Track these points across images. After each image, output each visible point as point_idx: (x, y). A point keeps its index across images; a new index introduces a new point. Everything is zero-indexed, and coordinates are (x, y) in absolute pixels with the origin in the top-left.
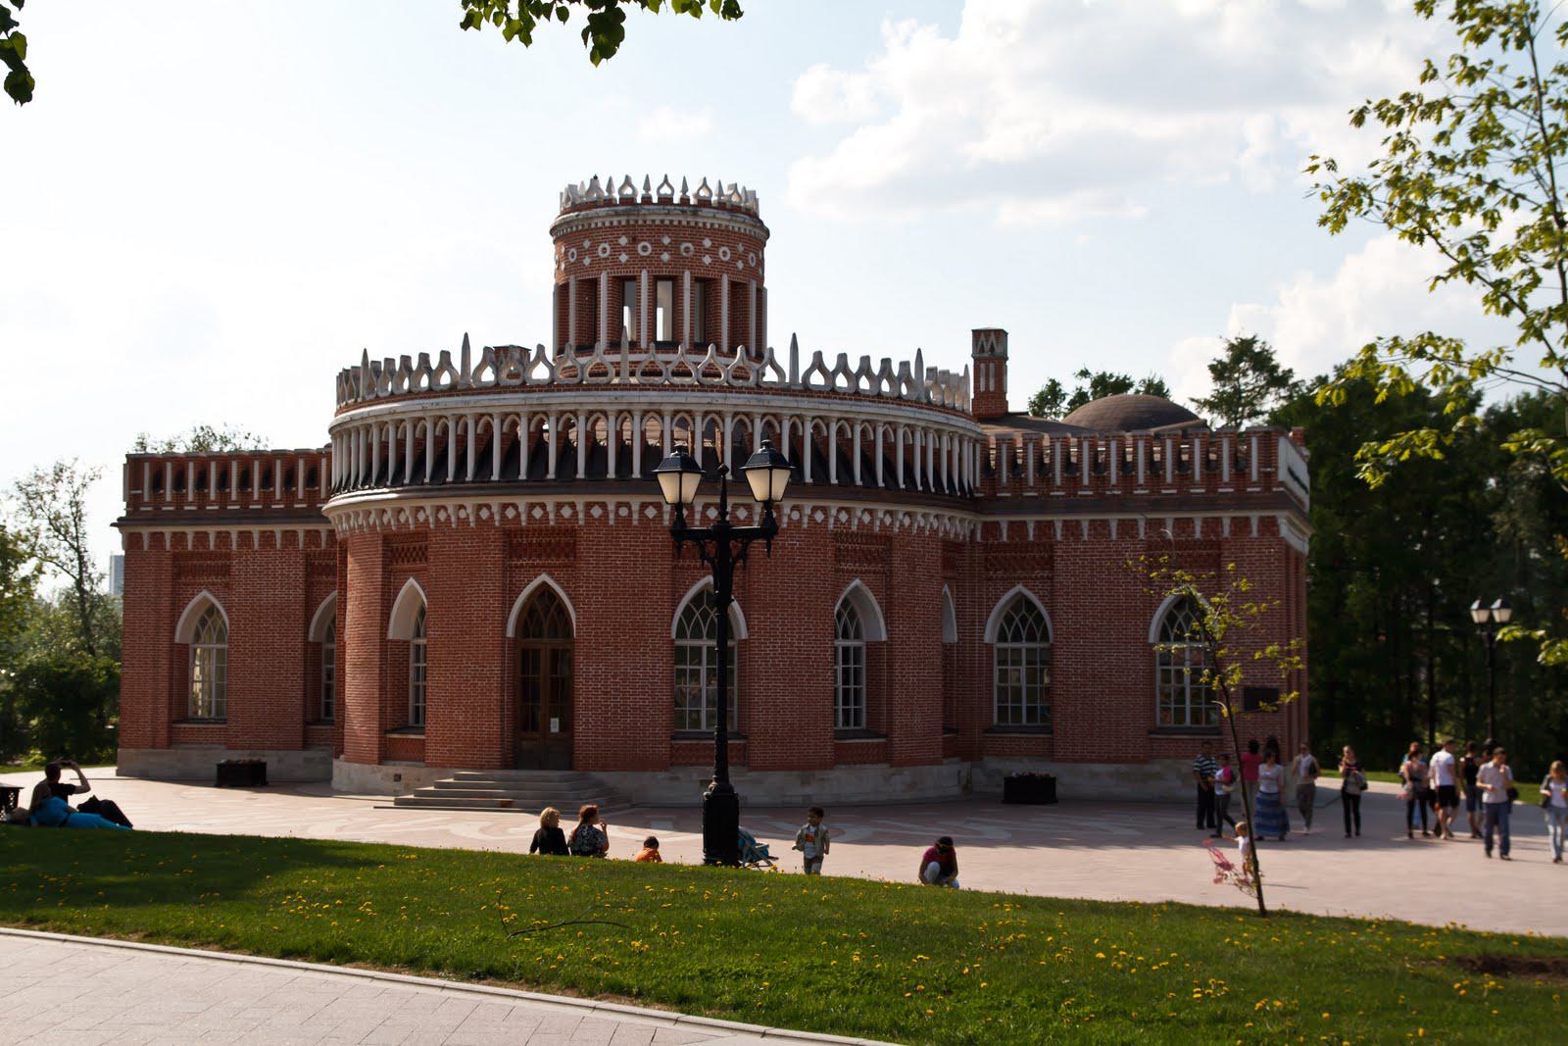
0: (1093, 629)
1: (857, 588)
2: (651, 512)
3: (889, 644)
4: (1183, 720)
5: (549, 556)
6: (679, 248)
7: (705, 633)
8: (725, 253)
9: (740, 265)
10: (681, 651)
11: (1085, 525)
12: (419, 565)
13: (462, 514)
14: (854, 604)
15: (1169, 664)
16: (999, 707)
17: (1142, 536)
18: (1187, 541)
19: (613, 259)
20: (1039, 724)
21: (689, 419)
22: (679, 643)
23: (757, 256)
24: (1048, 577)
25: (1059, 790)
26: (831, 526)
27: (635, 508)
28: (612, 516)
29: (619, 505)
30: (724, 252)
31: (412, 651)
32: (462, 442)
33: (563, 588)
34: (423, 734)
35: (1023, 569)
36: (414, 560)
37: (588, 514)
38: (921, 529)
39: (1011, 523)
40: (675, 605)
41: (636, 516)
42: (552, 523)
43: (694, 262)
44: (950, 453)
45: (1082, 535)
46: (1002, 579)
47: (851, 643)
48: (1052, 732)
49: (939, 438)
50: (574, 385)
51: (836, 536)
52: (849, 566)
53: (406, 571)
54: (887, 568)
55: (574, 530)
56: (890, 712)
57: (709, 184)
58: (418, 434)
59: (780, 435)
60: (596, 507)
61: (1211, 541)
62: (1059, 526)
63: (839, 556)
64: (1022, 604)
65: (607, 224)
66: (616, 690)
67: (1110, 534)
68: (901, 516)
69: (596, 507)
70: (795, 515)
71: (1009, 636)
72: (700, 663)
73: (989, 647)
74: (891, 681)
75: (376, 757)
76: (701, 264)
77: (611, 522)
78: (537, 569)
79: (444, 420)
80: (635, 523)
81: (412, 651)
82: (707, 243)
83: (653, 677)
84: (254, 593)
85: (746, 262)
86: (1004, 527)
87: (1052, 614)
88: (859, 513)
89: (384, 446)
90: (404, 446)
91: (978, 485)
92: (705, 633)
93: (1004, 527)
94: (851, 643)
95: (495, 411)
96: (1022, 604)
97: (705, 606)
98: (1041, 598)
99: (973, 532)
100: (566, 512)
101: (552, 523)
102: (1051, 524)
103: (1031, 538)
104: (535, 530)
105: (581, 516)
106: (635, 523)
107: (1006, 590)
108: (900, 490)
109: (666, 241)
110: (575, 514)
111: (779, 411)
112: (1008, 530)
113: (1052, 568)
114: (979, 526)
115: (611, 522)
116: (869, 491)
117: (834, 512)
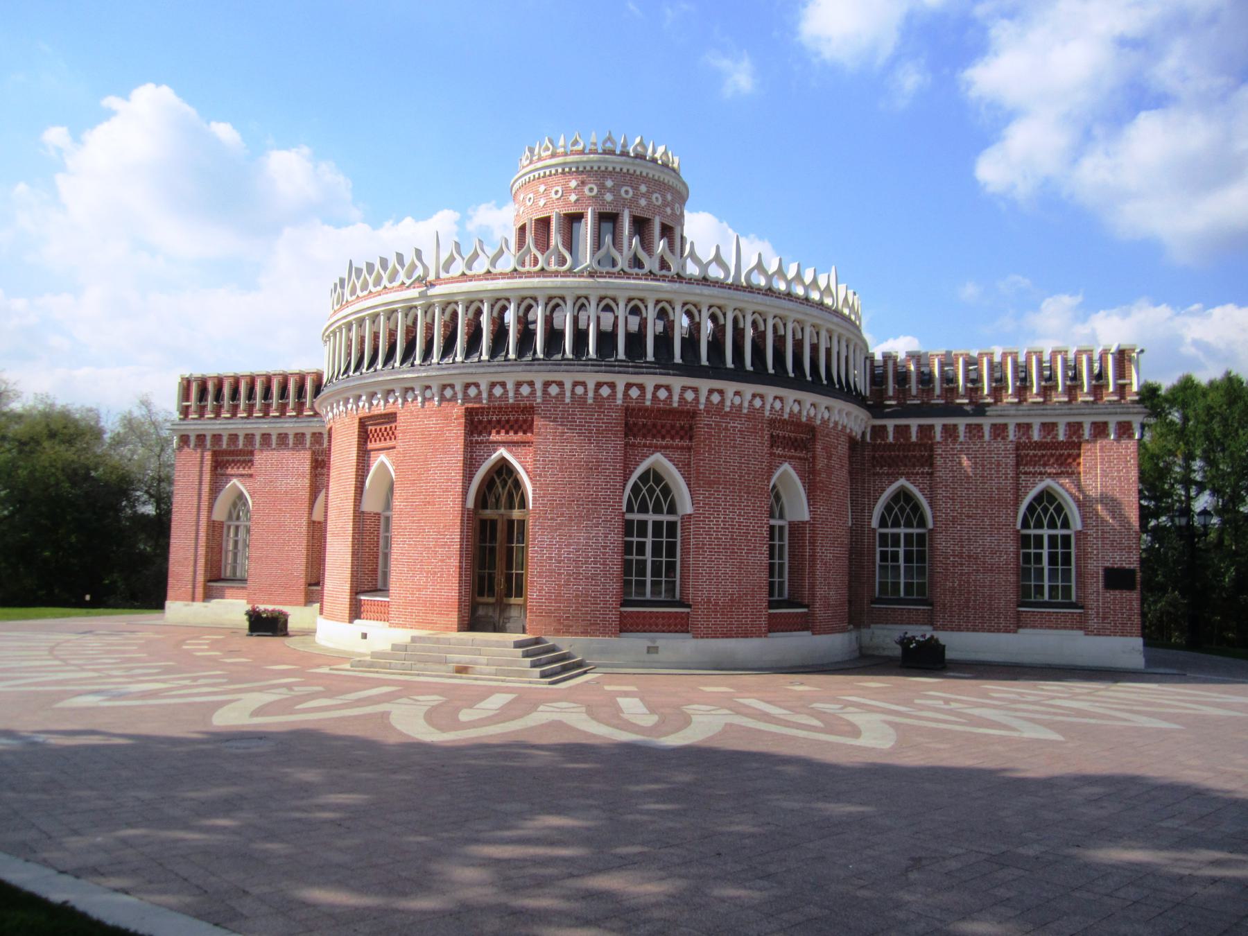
0: (969, 517)
1: (785, 472)
2: (605, 391)
3: (812, 524)
4: (1042, 595)
5: (516, 433)
6: (620, 190)
7: (651, 508)
8: (627, 192)
9: (669, 210)
10: (883, 537)
11: (962, 429)
12: (389, 443)
13: (579, 390)
14: (780, 488)
15: (892, 567)
16: (1070, 564)
17: (1011, 437)
18: (1052, 442)
19: (634, 201)
20: (915, 597)
21: (642, 306)
22: (629, 516)
23: (681, 208)
24: (928, 473)
25: (949, 655)
26: (767, 413)
27: (591, 386)
28: (568, 394)
29: (575, 384)
30: (657, 198)
31: (382, 520)
32: (429, 328)
33: (520, 462)
34: (388, 597)
35: (905, 466)
36: (385, 439)
37: (545, 392)
38: (836, 423)
39: (896, 427)
40: (626, 480)
41: (591, 394)
42: (511, 401)
43: (660, 210)
44: (828, 351)
45: (958, 437)
46: (888, 474)
47: (665, 518)
48: (931, 604)
49: (830, 338)
50: (534, 272)
51: (772, 422)
52: (779, 451)
53: (656, 447)
54: (810, 454)
55: (532, 407)
56: (812, 586)
57: (654, 271)
58: (429, 320)
59: (724, 326)
60: (554, 385)
61: (1074, 442)
62: (938, 430)
63: (630, 430)
64: (903, 496)
65: (567, 170)
66: (569, 559)
67: (983, 436)
68: (823, 409)
69: (554, 385)
70: (737, 400)
71: (1032, 525)
72: (645, 536)
73: (874, 530)
74: (813, 556)
75: (347, 615)
76: (638, 206)
77: (567, 400)
78: (894, 477)
79: (413, 311)
80: (590, 401)
81: (382, 520)
82: (643, 188)
83: (605, 548)
84: (271, 482)
85: (673, 209)
86: (890, 430)
87: (931, 505)
88: (808, 406)
89: (376, 336)
90: (378, 337)
91: (868, 394)
92: (651, 508)
93: (890, 430)
94: (915, 531)
95: (496, 571)
96: (903, 496)
97: (651, 483)
98: (921, 490)
99: (864, 434)
100: (525, 390)
101: (511, 401)
102: (931, 427)
103: (914, 439)
104: (495, 408)
105: (539, 393)
106: (590, 401)
107: (891, 483)
108: (822, 385)
109: (609, 183)
110: (533, 393)
111: (456, 674)
112: (894, 433)
113: (931, 465)
114: (869, 430)
115: (567, 400)
116: (798, 383)
117: (770, 399)
